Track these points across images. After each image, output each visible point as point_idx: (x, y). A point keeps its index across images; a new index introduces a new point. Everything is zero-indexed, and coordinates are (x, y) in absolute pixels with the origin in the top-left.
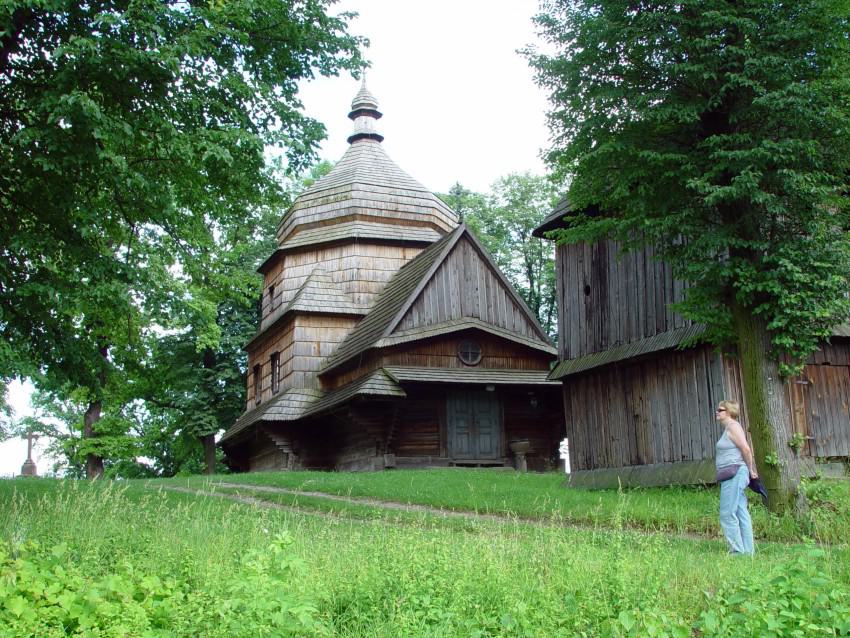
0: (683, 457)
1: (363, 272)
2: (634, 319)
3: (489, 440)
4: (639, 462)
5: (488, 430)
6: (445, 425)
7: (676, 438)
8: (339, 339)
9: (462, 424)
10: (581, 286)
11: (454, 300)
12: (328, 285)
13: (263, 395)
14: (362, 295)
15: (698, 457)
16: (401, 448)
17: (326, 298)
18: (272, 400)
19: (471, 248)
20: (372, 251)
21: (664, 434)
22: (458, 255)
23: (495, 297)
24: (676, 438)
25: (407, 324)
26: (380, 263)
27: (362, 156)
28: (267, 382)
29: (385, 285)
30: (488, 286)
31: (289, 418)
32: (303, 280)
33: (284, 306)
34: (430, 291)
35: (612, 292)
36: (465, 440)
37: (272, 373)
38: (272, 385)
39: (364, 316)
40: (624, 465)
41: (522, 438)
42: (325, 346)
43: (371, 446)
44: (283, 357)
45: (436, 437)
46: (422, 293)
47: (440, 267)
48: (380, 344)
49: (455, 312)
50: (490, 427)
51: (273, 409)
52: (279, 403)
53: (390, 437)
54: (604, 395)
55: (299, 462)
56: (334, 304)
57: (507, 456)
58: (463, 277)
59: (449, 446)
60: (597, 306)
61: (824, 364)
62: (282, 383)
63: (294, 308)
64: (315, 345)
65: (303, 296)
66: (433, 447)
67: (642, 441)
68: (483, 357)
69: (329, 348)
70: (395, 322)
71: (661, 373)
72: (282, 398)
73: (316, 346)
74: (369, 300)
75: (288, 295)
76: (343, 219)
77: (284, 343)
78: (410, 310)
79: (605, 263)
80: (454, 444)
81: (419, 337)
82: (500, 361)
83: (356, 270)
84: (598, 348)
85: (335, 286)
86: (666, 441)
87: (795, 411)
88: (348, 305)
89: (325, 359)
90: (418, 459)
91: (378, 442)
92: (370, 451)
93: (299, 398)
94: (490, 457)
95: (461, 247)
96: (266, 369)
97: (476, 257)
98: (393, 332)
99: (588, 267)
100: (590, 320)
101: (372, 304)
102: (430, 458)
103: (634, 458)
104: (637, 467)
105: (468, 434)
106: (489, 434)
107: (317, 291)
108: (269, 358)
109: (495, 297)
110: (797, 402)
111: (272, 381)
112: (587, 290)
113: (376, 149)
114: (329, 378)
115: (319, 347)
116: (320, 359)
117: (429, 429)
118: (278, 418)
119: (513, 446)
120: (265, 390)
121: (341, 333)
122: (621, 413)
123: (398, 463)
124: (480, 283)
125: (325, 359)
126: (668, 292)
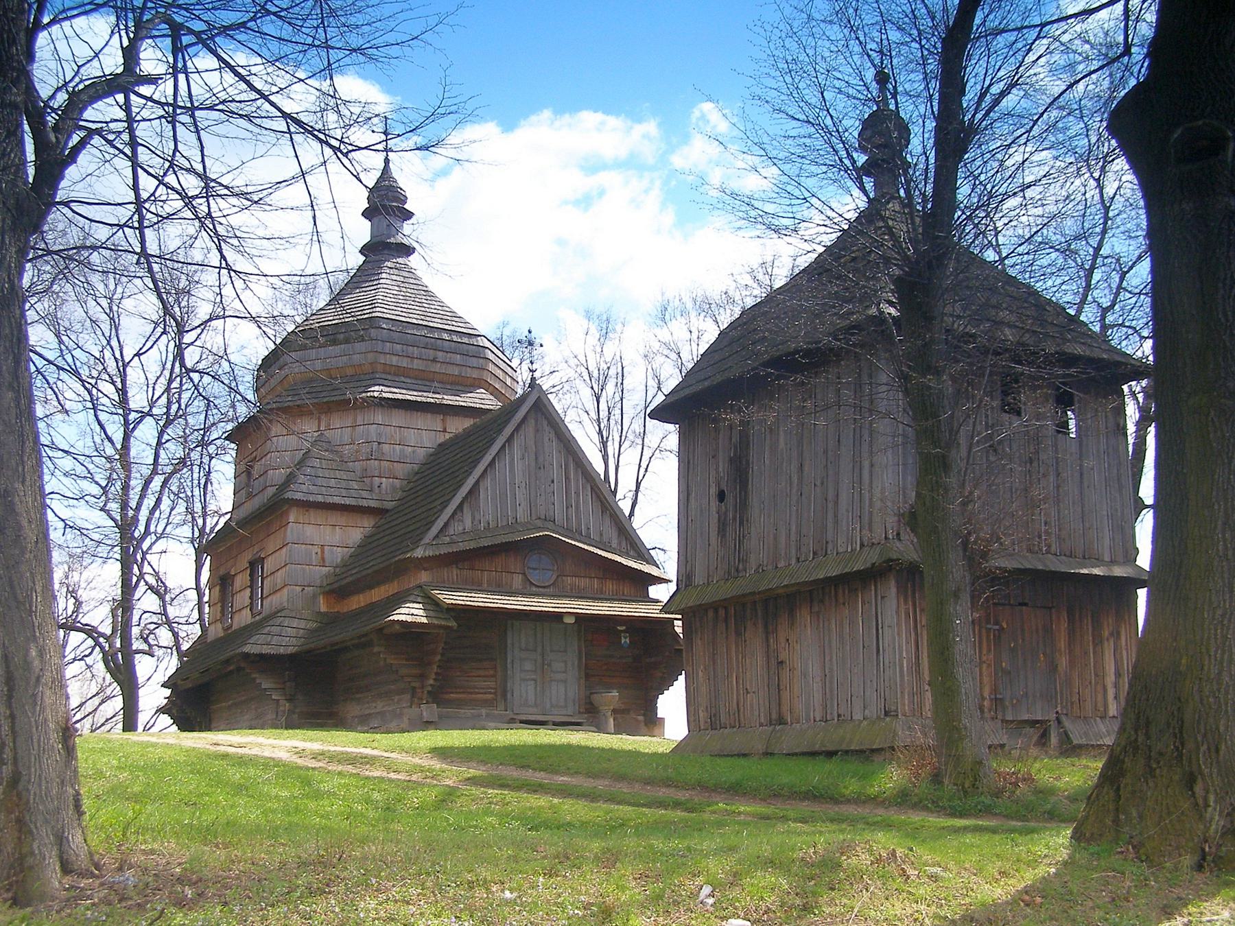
0: (839, 716)
1: (386, 447)
2: (783, 540)
3: (565, 686)
4: (781, 721)
6: (505, 669)
7: (831, 691)
8: (350, 542)
9: (528, 666)
10: (713, 491)
11: (521, 495)
13: (236, 617)
15: (858, 716)
16: (447, 696)
19: (545, 423)
20: (398, 418)
21: (817, 686)
23: (577, 493)
24: (831, 691)
25: (455, 528)
26: (411, 437)
27: (384, 275)
28: (243, 598)
29: (416, 467)
31: (282, 651)
33: (271, 491)
34: (488, 482)
35: (754, 501)
36: (531, 688)
39: (387, 511)
40: (761, 725)
41: (609, 687)
42: (332, 552)
43: (401, 692)
44: (269, 565)
45: (492, 684)
46: (477, 483)
47: (503, 446)
48: (419, 553)
52: (266, 631)
53: (431, 682)
54: (738, 633)
56: (344, 493)
57: (588, 711)
58: (533, 464)
59: (509, 696)
60: (734, 519)
61: (1021, 604)
63: (289, 495)
64: (316, 549)
66: (489, 696)
67: (786, 695)
69: (338, 555)
70: (440, 523)
71: (816, 609)
72: (271, 623)
74: (394, 488)
76: (836, 516)
77: (271, 545)
78: (460, 507)
79: (748, 462)
82: (583, 582)
84: (733, 573)
86: (818, 696)
87: (982, 662)
90: (468, 712)
91: (414, 688)
92: (400, 700)
93: (295, 623)
94: (564, 712)
96: (241, 580)
97: (552, 435)
98: (437, 536)
99: (723, 466)
100: (724, 536)
101: (399, 495)
102: (484, 711)
103: (774, 716)
104: (778, 728)
105: (535, 680)
106: (565, 681)
109: (577, 493)
110: (985, 652)
111: (251, 598)
112: (721, 496)
115: (323, 552)
117: (482, 673)
118: (266, 650)
119: (596, 699)
121: (354, 533)
122: (760, 659)
123: (440, 717)
124: (556, 473)
126: (830, 505)
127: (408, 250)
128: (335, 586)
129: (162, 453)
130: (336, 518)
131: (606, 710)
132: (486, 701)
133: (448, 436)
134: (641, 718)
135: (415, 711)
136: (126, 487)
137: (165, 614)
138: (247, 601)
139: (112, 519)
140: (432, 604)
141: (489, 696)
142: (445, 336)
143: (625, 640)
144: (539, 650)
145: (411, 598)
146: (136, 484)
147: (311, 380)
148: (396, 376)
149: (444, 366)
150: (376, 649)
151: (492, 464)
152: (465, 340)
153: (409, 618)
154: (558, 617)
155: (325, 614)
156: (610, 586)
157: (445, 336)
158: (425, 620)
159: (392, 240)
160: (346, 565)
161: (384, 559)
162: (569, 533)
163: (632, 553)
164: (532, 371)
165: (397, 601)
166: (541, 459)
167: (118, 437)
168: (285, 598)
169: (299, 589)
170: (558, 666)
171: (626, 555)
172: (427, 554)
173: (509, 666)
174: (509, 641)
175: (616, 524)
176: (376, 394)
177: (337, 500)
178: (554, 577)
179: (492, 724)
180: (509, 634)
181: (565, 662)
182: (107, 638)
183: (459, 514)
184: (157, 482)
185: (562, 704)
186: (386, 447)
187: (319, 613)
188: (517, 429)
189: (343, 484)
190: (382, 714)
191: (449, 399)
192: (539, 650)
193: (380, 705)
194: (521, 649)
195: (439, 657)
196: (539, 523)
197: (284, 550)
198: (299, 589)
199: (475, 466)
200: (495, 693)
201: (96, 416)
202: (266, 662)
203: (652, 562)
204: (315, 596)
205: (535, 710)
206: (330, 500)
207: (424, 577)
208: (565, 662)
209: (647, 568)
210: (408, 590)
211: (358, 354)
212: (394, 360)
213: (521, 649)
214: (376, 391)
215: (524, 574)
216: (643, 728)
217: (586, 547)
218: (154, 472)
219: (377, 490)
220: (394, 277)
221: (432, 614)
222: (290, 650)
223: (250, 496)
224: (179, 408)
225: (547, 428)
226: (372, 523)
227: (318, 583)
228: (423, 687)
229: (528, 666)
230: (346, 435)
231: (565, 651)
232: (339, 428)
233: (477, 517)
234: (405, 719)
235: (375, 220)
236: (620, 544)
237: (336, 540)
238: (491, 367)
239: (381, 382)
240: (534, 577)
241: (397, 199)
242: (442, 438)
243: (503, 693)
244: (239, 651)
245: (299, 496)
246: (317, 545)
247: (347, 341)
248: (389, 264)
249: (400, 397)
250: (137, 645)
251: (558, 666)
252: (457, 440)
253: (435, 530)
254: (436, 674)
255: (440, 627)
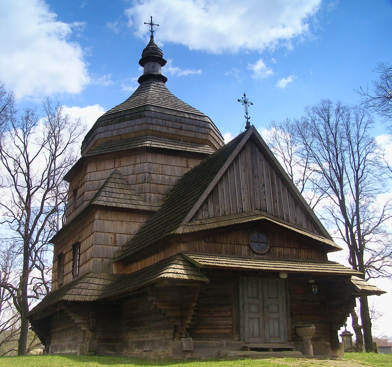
1: (153, 176)
3: (278, 326)
5: (275, 315)
8: (132, 232)
9: (254, 309)
12: (123, 187)
13: (65, 279)
14: (152, 195)
17: (122, 196)
18: (72, 282)
19: (257, 150)
20: (161, 159)
22: (248, 153)
25: (203, 214)
26: (168, 170)
27: (151, 89)
28: (69, 267)
29: (171, 187)
30: (273, 184)
31: (88, 299)
32: (103, 182)
33: (86, 204)
34: (223, 185)
37: (73, 260)
38: (73, 270)
42: (121, 237)
44: (83, 246)
46: (216, 186)
47: (232, 163)
48: (180, 231)
49: (245, 206)
50: (278, 312)
51: (74, 291)
52: (78, 286)
53: (189, 321)
55: (95, 339)
58: (251, 174)
59: (241, 330)
62: (81, 269)
63: (96, 202)
64: (111, 235)
65: (103, 193)
66: (228, 331)
68: (270, 247)
69: (124, 239)
70: (193, 212)
72: (82, 281)
73: (113, 237)
74: (158, 200)
75: (89, 195)
78: (206, 201)
80: (246, 328)
81: (215, 226)
82: (286, 251)
83: (147, 174)
85: (129, 187)
88: (141, 203)
89: (121, 248)
91: (176, 326)
92: (165, 334)
93: (97, 281)
94: (279, 341)
95: (250, 148)
96: (68, 257)
97: (262, 157)
98: (191, 220)
101: (161, 203)
102: (224, 342)
105: (258, 319)
106: (278, 319)
107: (114, 190)
108: (71, 247)
113: (162, 86)
114: (125, 259)
116: (116, 248)
117: (223, 314)
118: (78, 298)
119: (301, 331)
120: (67, 274)
123: (195, 346)
124: (266, 180)
125: (121, 248)
127: (164, 80)
128: (122, 257)
129: (45, 204)
130: (122, 217)
131: (308, 339)
132: (226, 334)
133: (189, 169)
134: (328, 343)
135: (177, 342)
136: (28, 220)
137: (43, 279)
138: (71, 268)
139: (21, 234)
140: (190, 265)
141: (228, 331)
142: (187, 116)
143: (315, 290)
144: (261, 297)
145: (176, 261)
146: (33, 217)
147: (111, 141)
148: (160, 136)
149: (186, 132)
150: (150, 299)
151: (225, 174)
152: (198, 118)
153: (175, 276)
154: (276, 274)
155: (116, 275)
156: (303, 253)
157: (187, 116)
158: (186, 277)
159: (155, 73)
160: (129, 245)
161: (157, 237)
162: (276, 217)
163: (315, 232)
164: (248, 119)
165: (165, 264)
166: (256, 171)
167: (25, 198)
168: (91, 266)
169: (100, 260)
170: (273, 308)
171: (312, 232)
172: (185, 231)
173: (241, 309)
174: (241, 292)
175: (304, 212)
176: (148, 145)
177: (124, 206)
178: (268, 247)
179: (232, 353)
180: (240, 287)
181: (278, 305)
182: (16, 290)
183: (205, 206)
184: (43, 217)
185: (277, 334)
186: (153, 176)
187: (112, 275)
188: (240, 152)
189: (128, 197)
190: (152, 342)
191: (189, 149)
192: (261, 297)
193: (150, 336)
194: (249, 297)
195: (194, 304)
196: (257, 212)
197: (92, 236)
198: (100, 260)
199: (215, 175)
200: (232, 329)
201: (16, 187)
202: (79, 306)
203: (331, 238)
204: (109, 265)
205: (259, 340)
206: (120, 206)
207: (182, 248)
208: (278, 305)
209: (327, 241)
210: (172, 257)
211: (137, 125)
212: (158, 128)
213: (249, 297)
214: (148, 143)
215: (249, 246)
216: (331, 352)
217: (289, 227)
218: (41, 213)
219: (148, 200)
220: (157, 90)
221: (190, 272)
222: (93, 298)
223: (75, 208)
224: (54, 183)
225: (258, 153)
226: (145, 220)
227: (112, 256)
228: (182, 325)
229: (254, 309)
230: (130, 169)
231: (277, 298)
232: (126, 167)
233: (217, 208)
234: (170, 349)
235: (146, 65)
236: (307, 225)
237: (125, 230)
238: (212, 134)
239: (150, 139)
240: (255, 247)
241: (157, 54)
242: (186, 171)
243: (237, 328)
244: (61, 299)
245: (101, 203)
246: (112, 233)
247: (131, 119)
248: (154, 85)
249: (162, 147)
250: (29, 293)
251: (273, 308)
252: (195, 170)
253: (190, 216)
254: (193, 316)
255: (196, 282)
